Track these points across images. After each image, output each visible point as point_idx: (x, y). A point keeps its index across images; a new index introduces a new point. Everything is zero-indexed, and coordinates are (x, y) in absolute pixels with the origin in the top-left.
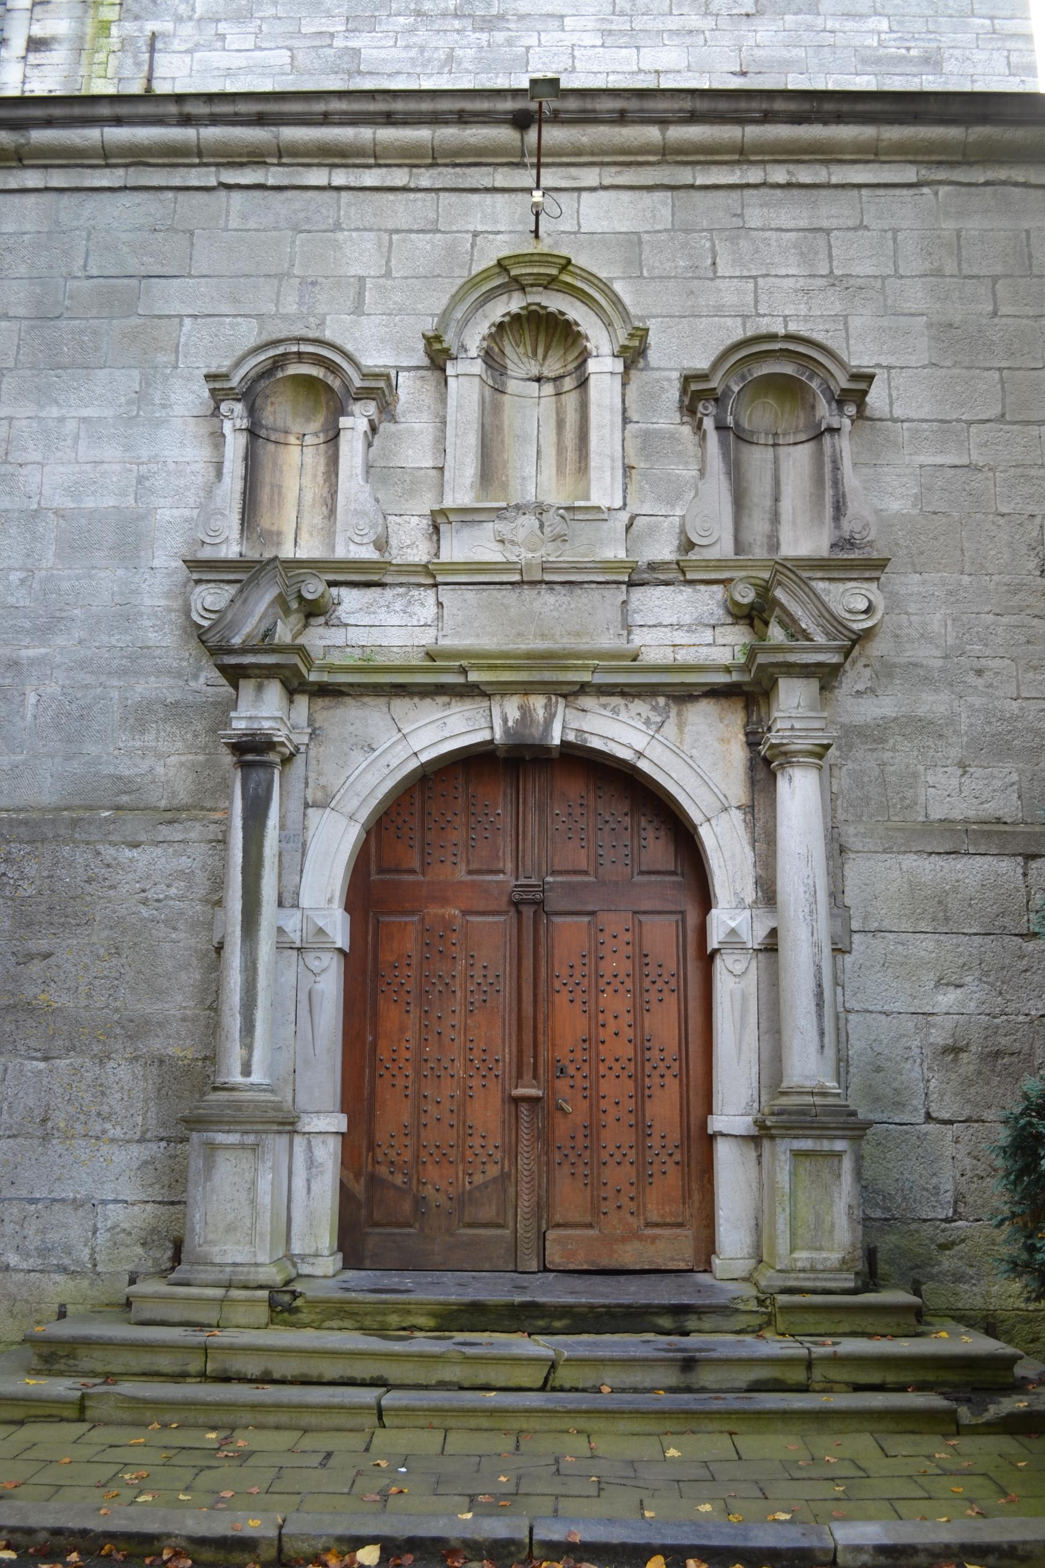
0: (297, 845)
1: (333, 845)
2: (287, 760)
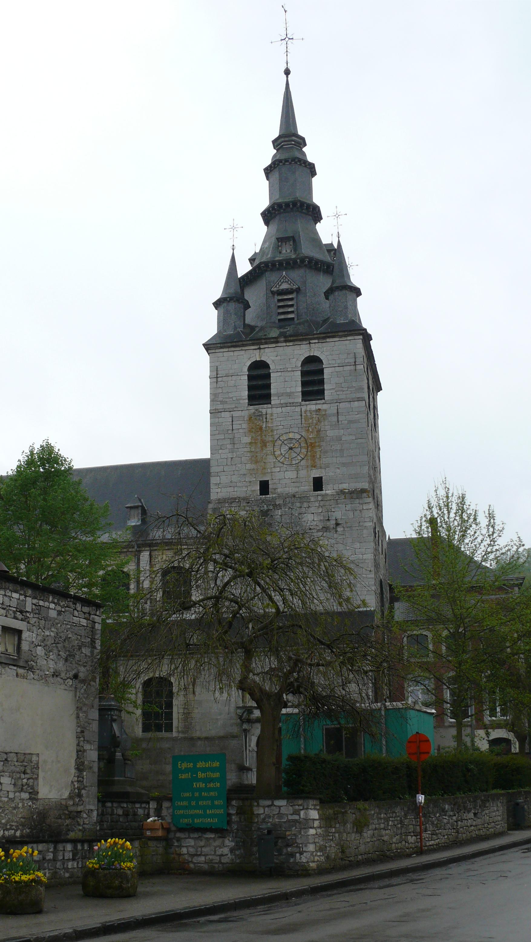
0: (250, 740)
1: (254, 740)
2: (249, 731)
